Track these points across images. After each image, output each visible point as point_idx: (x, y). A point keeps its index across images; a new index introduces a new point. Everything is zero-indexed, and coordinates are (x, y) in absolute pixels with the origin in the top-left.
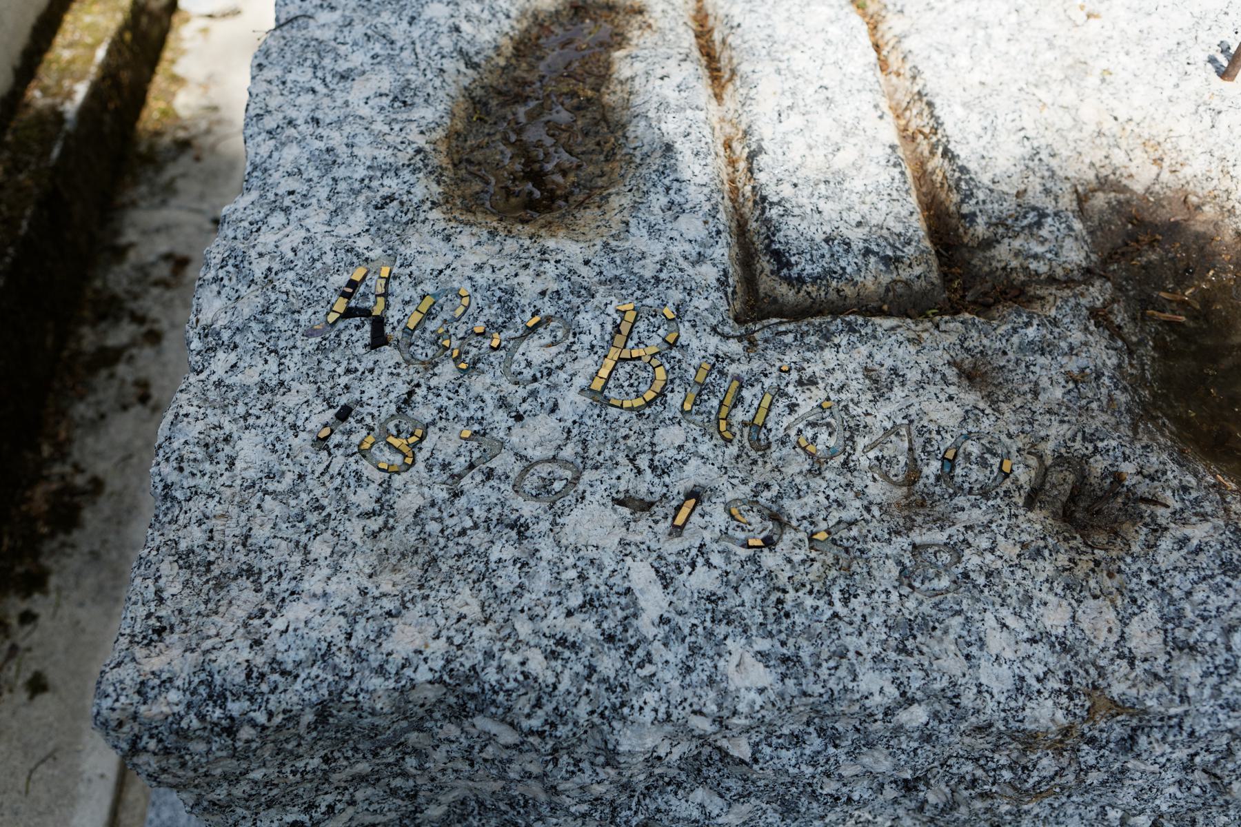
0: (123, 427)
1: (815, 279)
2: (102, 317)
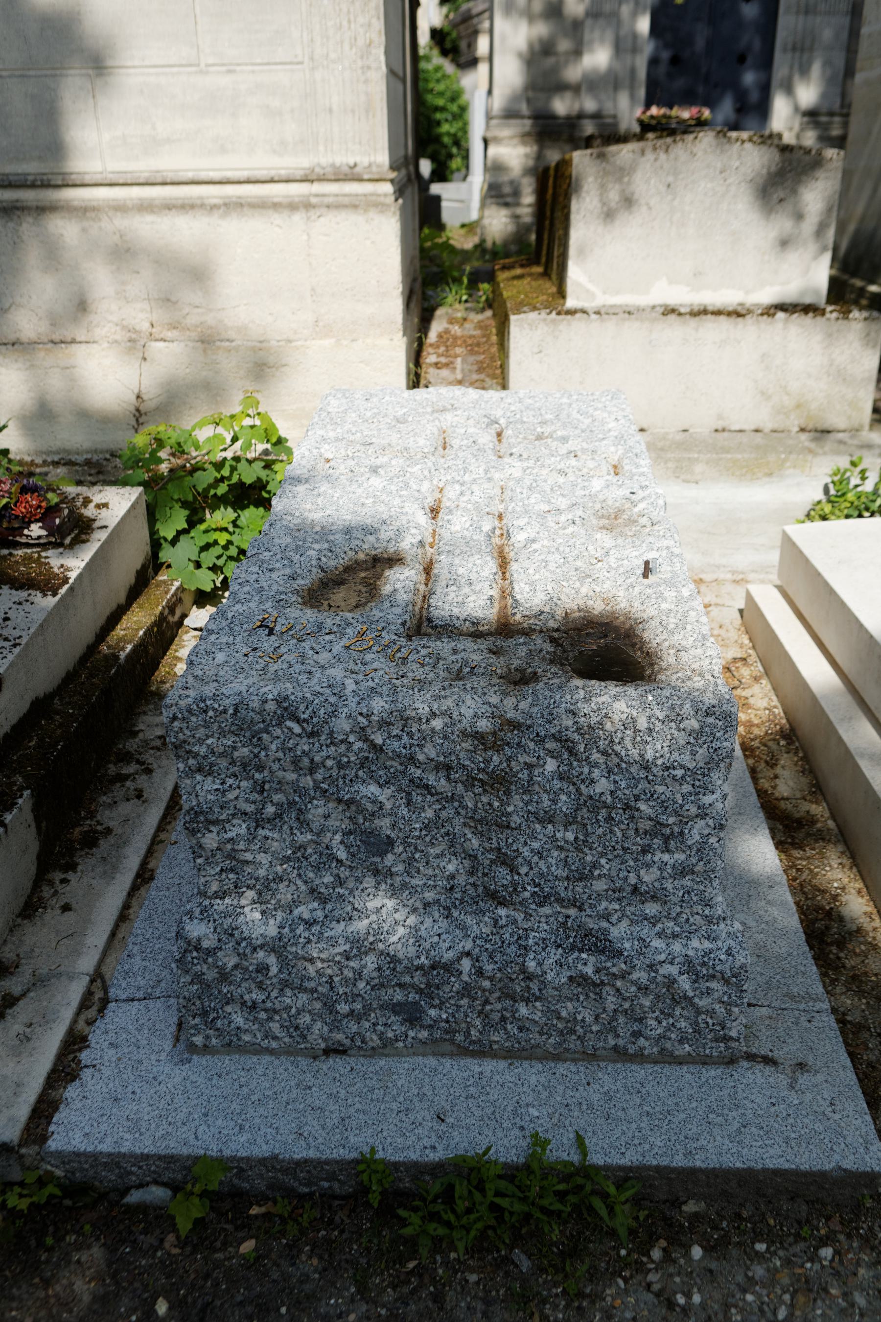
0: (126, 808)
1: (441, 626)
2: (122, 761)
